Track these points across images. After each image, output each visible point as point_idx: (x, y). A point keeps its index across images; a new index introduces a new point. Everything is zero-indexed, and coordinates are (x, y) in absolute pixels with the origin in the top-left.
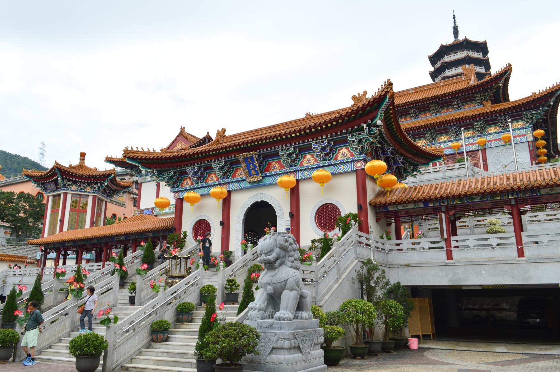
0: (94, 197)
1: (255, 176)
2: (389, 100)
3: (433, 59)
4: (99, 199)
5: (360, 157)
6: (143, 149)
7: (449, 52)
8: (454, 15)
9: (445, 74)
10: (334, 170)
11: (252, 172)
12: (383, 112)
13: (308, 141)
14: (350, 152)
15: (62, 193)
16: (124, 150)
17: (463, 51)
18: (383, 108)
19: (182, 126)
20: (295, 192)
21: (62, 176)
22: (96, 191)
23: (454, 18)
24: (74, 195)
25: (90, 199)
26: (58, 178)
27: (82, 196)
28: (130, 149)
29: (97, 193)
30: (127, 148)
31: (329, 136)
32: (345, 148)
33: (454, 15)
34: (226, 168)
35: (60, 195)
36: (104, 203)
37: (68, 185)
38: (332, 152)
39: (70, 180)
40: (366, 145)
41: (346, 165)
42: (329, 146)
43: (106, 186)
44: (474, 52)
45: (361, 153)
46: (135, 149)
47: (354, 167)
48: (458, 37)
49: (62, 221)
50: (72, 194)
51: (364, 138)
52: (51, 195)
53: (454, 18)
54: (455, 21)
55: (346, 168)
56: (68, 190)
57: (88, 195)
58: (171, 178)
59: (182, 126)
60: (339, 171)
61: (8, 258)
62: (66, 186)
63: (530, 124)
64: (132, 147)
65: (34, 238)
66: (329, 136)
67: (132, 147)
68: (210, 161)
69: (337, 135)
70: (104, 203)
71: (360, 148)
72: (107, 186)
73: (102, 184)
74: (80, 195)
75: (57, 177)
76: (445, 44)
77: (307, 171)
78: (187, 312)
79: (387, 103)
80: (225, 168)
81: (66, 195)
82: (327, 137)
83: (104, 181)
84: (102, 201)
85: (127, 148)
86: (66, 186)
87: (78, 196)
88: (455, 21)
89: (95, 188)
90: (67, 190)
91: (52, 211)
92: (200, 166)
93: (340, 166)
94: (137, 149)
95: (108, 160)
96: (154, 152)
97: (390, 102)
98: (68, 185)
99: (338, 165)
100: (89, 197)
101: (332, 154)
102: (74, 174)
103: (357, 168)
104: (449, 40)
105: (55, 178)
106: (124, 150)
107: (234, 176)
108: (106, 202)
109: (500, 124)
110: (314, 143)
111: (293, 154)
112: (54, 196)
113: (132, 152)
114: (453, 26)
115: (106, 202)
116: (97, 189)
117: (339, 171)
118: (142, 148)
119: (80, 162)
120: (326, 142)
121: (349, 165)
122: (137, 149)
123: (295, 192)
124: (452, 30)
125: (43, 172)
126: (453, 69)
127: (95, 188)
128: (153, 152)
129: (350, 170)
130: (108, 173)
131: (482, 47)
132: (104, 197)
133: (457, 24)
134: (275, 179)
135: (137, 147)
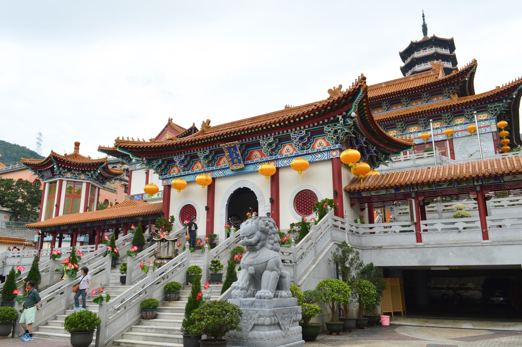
0: (88, 184)
1: (238, 164)
2: (362, 94)
3: (404, 55)
4: (92, 186)
5: (335, 147)
6: (134, 139)
7: (419, 48)
8: (423, 14)
9: (415, 69)
10: (312, 159)
11: (235, 160)
12: (357, 104)
13: (287, 132)
14: (326, 141)
15: (58, 180)
16: (115, 140)
17: (431, 47)
18: (357, 101)
19: (169, 118)
20: (275, 179)
21: (58, 164)
22: (90, 178)
23: (423, 16)
24: (69, 182)
25: (84, 186)
26: (54, 166)
27: (76, 183)
28: (121, 139)
29: (91, 180)
30: (118, 138)
31: (307, 126)
32: (322, 138)
33: (423, 14)
34: (211, 157)
35: (56, 182)
36: (97, 189)
37: (64, 173)
38: (214, 160)
39: (66, 168)
40: (342, 135)
41: (323, 154)
42: (307, 137)
43: (99, 173)
44: (442, 48)
45: (336, 143)
46: (126, 139)
47: (330, 156)
48: (427, 34)
49: (58, 206)
50: (67, 181)
51: (339, 129)
52: (47, 182)
53: (423, 16)
54: (424, 19)
55: (323, 157)
56: (64, 177)
57: (82, 182)
58: (160, 166)
59: (169, 118)
60: (316, 159)
61: (8, 241)
62: (62, 174)
63: (494, 116)
64: (123, 137)
65: (32, 222)
66: (307, 126)
67: (123, 137)
68: (195, 150)
69: (314, 126)
70: (97, 189)
71: (335, 138)
72: (100, 174)
73: (95, 171)
74: (75, 182)
75: (53, 165)
76: (414, 41)
77: (286, 159)
78: (174, 291)
79: (361, 96)
80: (210, 157)
81: (61, 182)
82: (305, 128)
83: (97, 169)
84: (95, 187)
85: (118, 138)
86: (62, 174)
87: (73, 183)
88: (424, 19)
89: (88, 175)
90: (63, 177)
91: (49, 197)
92: (186, 155)
93: (317, 155)
94: (128, 139)
95: (100, 150)
96: (144, 142)
97: (364, 95)
98: (64, 173)
99: (315, 154)
100: (83, 184)
101: (310, 144)
102: (69, 163)
103: (333, 156)
104: (419, 37)
105: (51, 166)
106: (115, 140)
107: (218, 164)
108: (99, 188)
109: (466, 116)
110: (293, 134)
111: (273, 144)
112: (50, 183)
113: (123, 141)
114: (422, 24)
115: (99, 188)
116: (90, 177)
117: (316, 159)
118: (132, 138)
119: (74, 151)
120: (304, 133)
121: (326, 154)
122: (128, 139)
123: (275, 179)
124: (421, 28)
125: (40, 161)
126: (423, 65)
127: (88, 175)
128: (142, 142)
129: (326, 158)
130: (100, 162)
131: (450, 44)
132: (97, 183)
133: (426, 22)
134: (256, 167)
135: (128, 137)
